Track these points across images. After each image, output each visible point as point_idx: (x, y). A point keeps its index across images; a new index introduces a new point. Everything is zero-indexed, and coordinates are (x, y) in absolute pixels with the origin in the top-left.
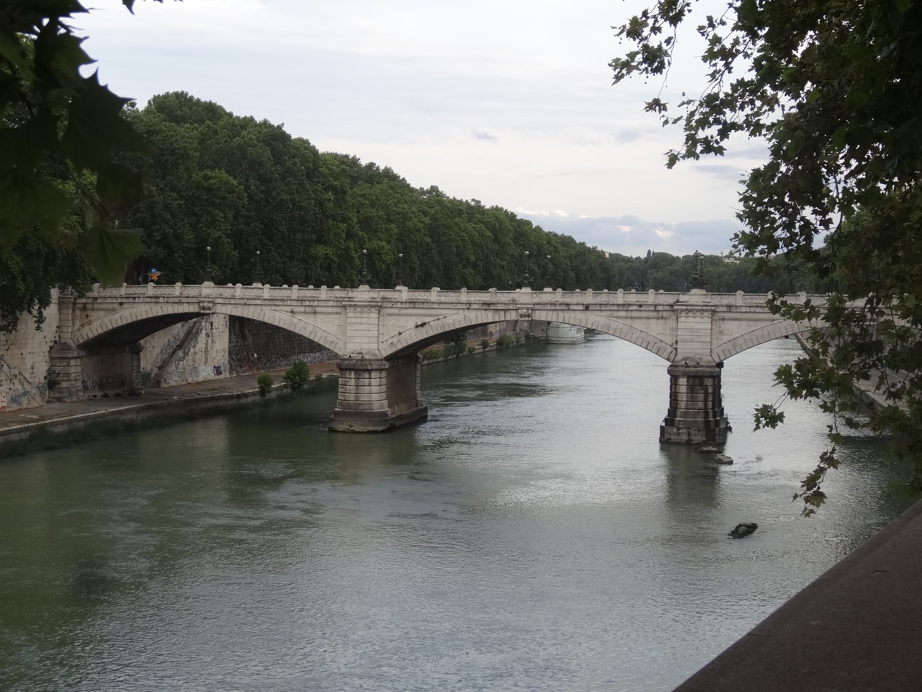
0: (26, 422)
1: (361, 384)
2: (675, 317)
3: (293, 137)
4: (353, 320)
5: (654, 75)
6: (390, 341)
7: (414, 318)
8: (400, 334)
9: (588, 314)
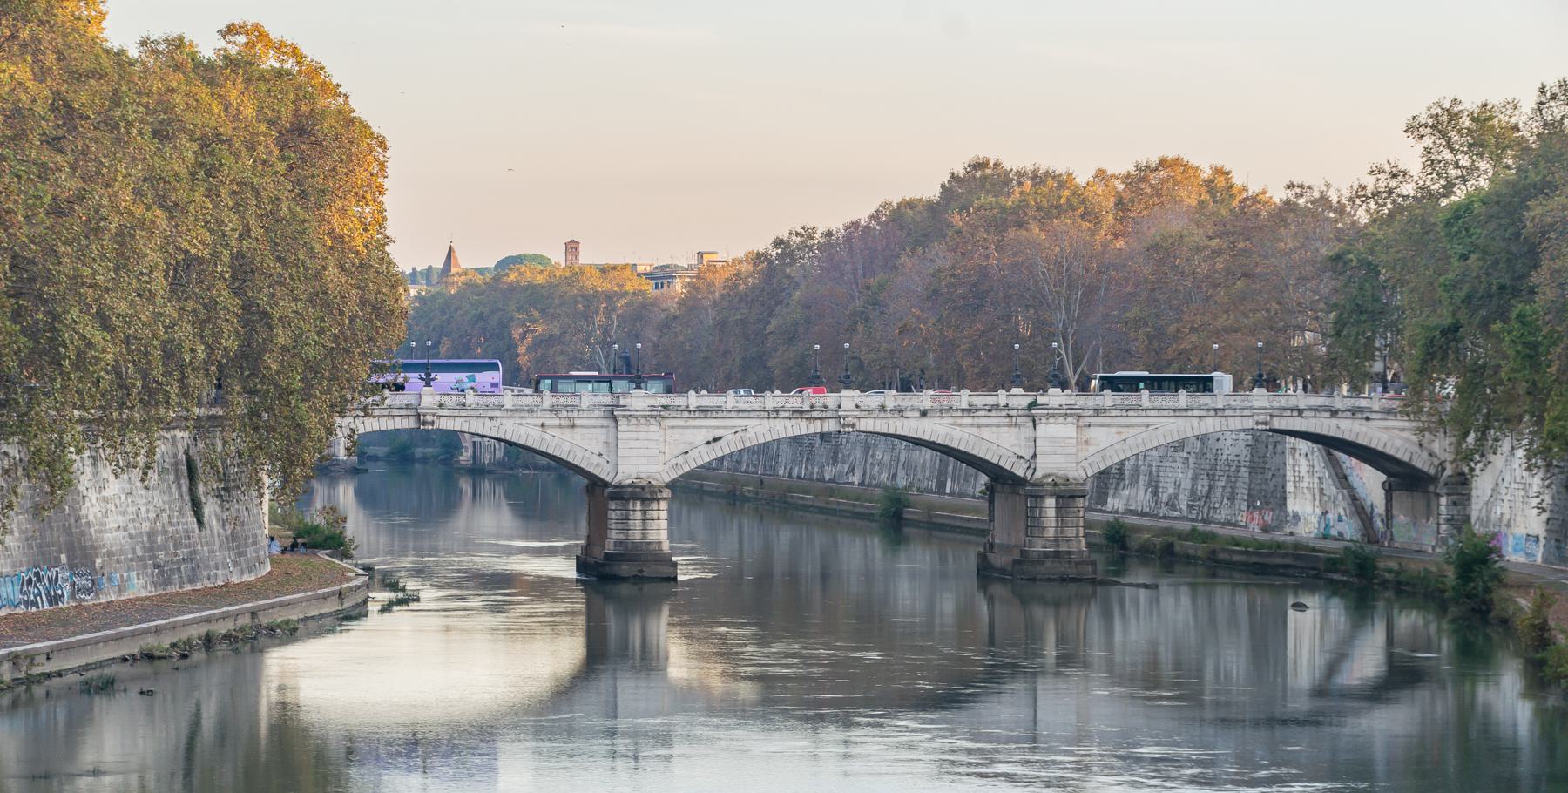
2: (1031, 423)
5: (572, 247)
6: (674, 461)
7: (704, 431)
9: (925, 421)
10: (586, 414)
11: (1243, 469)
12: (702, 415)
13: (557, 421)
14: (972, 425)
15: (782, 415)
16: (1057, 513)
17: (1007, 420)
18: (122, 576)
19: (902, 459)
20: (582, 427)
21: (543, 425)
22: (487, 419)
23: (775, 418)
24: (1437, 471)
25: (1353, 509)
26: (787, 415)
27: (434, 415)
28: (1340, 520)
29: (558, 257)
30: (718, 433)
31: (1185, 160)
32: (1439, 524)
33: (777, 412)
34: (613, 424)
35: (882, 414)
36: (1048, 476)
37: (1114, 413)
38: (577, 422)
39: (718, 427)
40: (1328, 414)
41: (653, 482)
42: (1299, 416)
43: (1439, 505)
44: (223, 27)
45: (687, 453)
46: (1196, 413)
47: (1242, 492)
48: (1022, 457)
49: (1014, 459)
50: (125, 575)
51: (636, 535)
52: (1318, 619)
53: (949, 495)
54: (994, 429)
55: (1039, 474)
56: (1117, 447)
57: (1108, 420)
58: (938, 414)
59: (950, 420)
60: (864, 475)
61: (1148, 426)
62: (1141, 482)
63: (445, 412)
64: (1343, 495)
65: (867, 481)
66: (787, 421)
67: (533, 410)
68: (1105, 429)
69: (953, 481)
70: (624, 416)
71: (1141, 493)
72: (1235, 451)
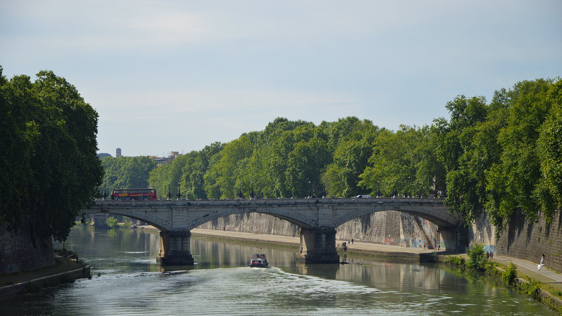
0: (180, 293)
1: (184, 243)
2: (317, 209)
3: (247, 133)
4: (176, 214)
5: (119, 151)
6: (192, 223)
7: (202, 213)
8: (196, 220)
9: (280, 208)
10: (161, 207)
11: (383, 224)
12: (202, 207)
13: (151, 210)
14: (296, 210)
15: (230, 206)
16: (326, 240)
17: (308, 208)
18: (10, 266)
19: (255, 222)
20: (159, 212)
21: (146, 211)
22: (126, 209)
23: (227, 208)
24: (456, 224)
25: (425, 237)
26: (231, 207)
27: (107, 208)
28: (420, 241)
29: (114, 155)
30: (207, 213)
31: (292, 121)
32: (457, 242)
33: (228, 206)
34: (171, 211)
35: (265, 206)
36: (323, 226)
37: (345, 205)
38: (158, 210)
39: (207, 211)
40: (419, 205)
41: (185, 231)
42: (409, 205)
43: (457, 236)
44: (38, 73)
45: (196, 220)
46: (374, 205)
47: (383, 232)
48: (313, 220)
49: (311, 221)
50: (11, 265)
51: (179, 249)
52: (424, 273)
53: (272, 234)
54: (304, 211)
55: (319, 226)
56: (346, 216)
57: (343, 207)
58: (284, 206)
59: (288, 208)
60: (240, 228)
61: (357, 209)
62: (345, 229)
63: (111, 207)
64: (421, 232)
65: (242, 230)
66: (232, 209)
67: (142, 206)
68: (342, 210)
69: (274, 229)
70: (174, 208)
71: (345, 233)
72: (380, 218)
